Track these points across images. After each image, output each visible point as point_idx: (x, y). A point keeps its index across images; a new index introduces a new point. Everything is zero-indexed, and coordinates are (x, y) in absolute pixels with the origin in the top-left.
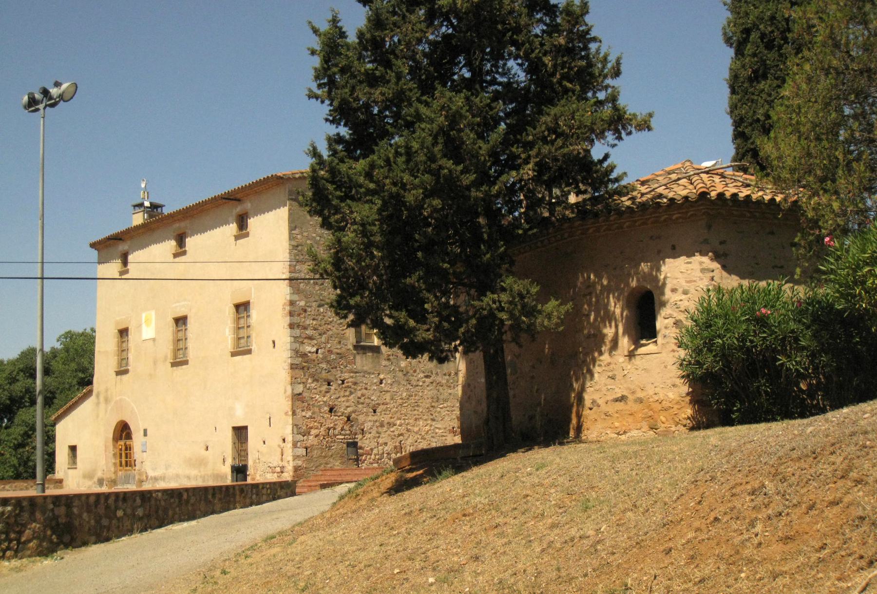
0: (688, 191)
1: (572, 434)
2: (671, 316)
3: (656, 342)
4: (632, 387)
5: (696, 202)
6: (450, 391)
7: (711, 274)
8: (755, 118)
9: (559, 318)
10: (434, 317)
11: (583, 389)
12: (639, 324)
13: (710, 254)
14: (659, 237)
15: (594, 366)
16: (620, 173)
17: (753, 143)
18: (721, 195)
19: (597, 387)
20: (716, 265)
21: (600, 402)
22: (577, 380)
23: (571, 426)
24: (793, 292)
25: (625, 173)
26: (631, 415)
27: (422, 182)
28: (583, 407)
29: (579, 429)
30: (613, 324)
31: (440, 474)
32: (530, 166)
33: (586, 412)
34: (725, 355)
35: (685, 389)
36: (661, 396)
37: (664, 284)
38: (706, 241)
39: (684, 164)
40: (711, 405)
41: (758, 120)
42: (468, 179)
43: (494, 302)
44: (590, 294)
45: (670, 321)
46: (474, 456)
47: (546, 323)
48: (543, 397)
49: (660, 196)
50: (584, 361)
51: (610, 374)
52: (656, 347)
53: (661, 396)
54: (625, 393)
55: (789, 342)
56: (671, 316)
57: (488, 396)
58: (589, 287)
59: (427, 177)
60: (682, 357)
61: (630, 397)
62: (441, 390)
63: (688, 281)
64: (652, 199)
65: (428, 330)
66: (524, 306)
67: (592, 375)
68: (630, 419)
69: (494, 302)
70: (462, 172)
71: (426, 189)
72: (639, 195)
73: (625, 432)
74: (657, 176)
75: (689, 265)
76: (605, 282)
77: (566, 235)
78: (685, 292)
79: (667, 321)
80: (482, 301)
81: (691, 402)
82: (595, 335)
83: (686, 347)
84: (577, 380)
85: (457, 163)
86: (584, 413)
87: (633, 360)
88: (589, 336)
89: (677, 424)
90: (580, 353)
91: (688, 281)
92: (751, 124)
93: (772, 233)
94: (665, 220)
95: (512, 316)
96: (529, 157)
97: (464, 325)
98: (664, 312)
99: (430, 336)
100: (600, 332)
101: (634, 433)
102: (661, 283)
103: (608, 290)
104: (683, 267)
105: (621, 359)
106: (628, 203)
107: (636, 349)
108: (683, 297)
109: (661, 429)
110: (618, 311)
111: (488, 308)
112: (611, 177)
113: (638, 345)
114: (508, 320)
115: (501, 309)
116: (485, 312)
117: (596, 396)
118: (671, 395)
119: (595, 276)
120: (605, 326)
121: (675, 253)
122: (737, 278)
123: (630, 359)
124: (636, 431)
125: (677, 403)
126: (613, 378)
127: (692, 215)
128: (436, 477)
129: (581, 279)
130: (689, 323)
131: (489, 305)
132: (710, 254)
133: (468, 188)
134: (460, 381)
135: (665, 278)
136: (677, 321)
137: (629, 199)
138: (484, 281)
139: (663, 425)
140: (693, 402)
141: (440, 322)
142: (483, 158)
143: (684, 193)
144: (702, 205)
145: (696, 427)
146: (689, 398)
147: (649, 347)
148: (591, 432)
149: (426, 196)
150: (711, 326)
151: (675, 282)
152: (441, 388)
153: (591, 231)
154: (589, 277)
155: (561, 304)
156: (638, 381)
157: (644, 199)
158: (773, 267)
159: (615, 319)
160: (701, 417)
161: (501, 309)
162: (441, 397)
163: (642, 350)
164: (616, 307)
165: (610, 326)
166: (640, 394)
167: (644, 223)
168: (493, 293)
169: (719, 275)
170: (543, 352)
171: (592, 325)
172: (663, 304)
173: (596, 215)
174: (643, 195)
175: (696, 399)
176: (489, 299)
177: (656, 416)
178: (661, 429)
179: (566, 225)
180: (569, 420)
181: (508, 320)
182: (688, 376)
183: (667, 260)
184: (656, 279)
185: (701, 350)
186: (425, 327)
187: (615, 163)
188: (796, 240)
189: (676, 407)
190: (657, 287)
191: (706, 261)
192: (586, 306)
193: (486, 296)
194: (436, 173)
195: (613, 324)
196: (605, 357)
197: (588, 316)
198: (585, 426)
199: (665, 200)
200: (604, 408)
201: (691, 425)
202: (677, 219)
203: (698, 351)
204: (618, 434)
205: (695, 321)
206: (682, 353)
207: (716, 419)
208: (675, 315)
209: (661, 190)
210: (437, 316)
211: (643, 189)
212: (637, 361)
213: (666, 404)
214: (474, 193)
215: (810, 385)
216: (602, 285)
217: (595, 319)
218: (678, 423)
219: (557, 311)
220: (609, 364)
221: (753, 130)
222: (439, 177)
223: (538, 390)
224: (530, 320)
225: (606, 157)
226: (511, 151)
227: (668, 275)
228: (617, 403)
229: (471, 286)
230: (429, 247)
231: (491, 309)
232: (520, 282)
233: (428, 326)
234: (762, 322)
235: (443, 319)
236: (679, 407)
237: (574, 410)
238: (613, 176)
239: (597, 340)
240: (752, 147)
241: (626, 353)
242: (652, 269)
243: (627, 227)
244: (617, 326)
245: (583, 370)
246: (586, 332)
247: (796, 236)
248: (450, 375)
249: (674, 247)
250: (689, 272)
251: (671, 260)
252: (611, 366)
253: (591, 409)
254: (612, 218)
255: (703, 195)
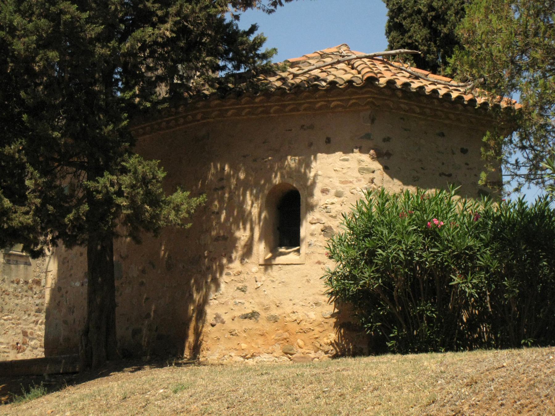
0: (351, 76)
1: (187, 353)
2: (319, 222)
3: (298, 251)
4: (266, 302)
5: (361, 88)
6: (17, 301)
7: (372, 175)
8: (416, 9)
9: (188, 212)
10: (36, 197)
11: (205, 301)
12: (278, 229)
13: (372, 152)
14: (312, 127)
15: (221, 274)
16: (270, 49)
17: (410, 37)
18: (391, 83)
19: (223, 300)
20: (377, 166)
21: (225, 317)
22: (198, 290)
23: (187, 345)
24: (462, 207)
25: (275, 50)
26: (262, 335)
27: (37, 29)
28: (203, 323)
29: (196, 349)
30: (248, 226)
31: (28, 391)
32: (168, 26)
33: (207, 329)
34: (385, 270)
35: (330, 309)
36: (300, 316)
37: (314, 183)
38: (368, 136)
39: (339, 48)
40: (362, 329)
41: (419, 12)
42: (94, 30)
43: (112, 185)
44: (223, 188)
45: (318, 227)
46: (66, 373)
47: (172, 217)
48: (153, 307)
49: (317, 78)
50: (209, 268)
51: (240, 285)
52: (298, 257)
53: (300, 316)
54: (256, 309)
55: (465, 260)
56: (319, 222)
57: (90, 301)
58: (222, 179)
59: (43, 22)
60: (332, 270)
61: (263, 314)
62: (7, 299)
63: (344, 181)
64: (308, 81)
65: (27, 213)
66: (148, 193)
67: (218, 286)
68: (260, 341)
69: (112, 185)
70: (88, 21)
71: (40, 37)
72: (291, 77)
73: (253, 356)
74: (309, 58)
75: (346, 163)
76: (242, 176)
77: (199, 117)
78: (338, 195)
79: (313, 227)
80: (98, 183)
81: (336, 325)
82: (225, 238)
83: (340, 259)
84: (198, 290)
85: (82, 9)
86: (204, 330)
87: (269, 271)
88: (217, 238)
89: (317, 350)
90: (205, 257)
91: (344, 181)
92: (410, 15)
93: (442, 135)
94: (320, 108)
95: (133, 204)
96: (167, 14)
97: (74, 211)
98: (310, 217)
99: (28, 220)
100: (232, 234)
101: (265, 358)
102: (309, 183)
103: (245, 185)
104: (339, 164)
105: (255, 269)
106: (279, 84)
107: (273, 258)
108: (336, 200)
109: (297, 355)
110: (255, 211)
111: (104, 191)
112: (259, 52)
113: (276, 254)
114: (127, 207)
115: (120, 193)
116: (100, 196)
117: (221, 311)
118: (312, 315)
119: (231, 167)
120: (238, 228)
121: (329, 147)
122: (400, 183)
123: (266, 270)
124: (267, 356)
125: (319, 325)
126: (243, 290)
127: (354, 104)
128: (23, 394)
129: (213, 171)
130: (344, 230)
131: (106, 187)
132: (372, 152)
133: (92, 41)
134: (49, 285)
135: (316, 176)
136: (326, 228)
137: (278, 80)
138: (102, 157)
139: (300, 350)
140: (339, 325)
141: (43, 204)
142: (113, 7)
143: (348, 77)
144: (366, 93)
145: (341, 352)
146: (334, 320)
147: (291, 257)
148: (212, 353)
149: (39, 47)
150: (370, 235)
151: (327, 181)
152: (7, 297)
153: (230, 113)
154: (223, 169)
155: (190, 197)
156: (273, 297)
157: (297, 81)
158: (440, 175)
159: (251, 220)
160: (348, 344)
161: (120, 193)
162: (6, 307)
163: (280, 260)
164: (253, 207)
165: (245, 229)
166: (275, 312)
167: (296, 109)
168: (112, 174)
169: (380, 178)
170: (159, 254)
171: (222, 226)
172: (311, 208)
173: (239, 94)
174: (295, 76)
175: (343, 323)
176: (105, 180)
177: (292, 339)
178: (297, 355)
179: (201, 104)
180: (185, 337)
181: (127, 207)
182: (337, 293)
183: (319, 155)
184: (304, 177)
185: (358, 263)
186: (26, 209)
187: (265, 36)
188: (485, 139)
189: (317, 329)
190: (306, 187)
191: (366, 159)
192: (216, 203)
193: (102, 176)
194: (55, 18)
195: (248, 226)
196: (236, 265)
197: (218, 214)
198: (204, 345)
199: (324, 84)
200: (230, 325)
201: (334, 352)
202: (336, 107)
203: (355, 264)
204: (244, 357)
205: (351, 228)
206: (332, 265)
207: (365, 347)
208: (324, 220)
209: (316, 72)
210: (39, 197)
211: (294, 70)
212: (274, 272)
213: (305, 325)
214: (100, 50)
215: (471, 315)
216: (238, 179)
217: (227, 219)
218: (318, 349)
219: (188, 203)
220: (239, 273)
221: (412, 22)
222: (59, 23)
223: (147, 299)
224: (154, 211)
225: (253, 29)
226: (145, 6)
227: (320, 173)
228: (246, 321)
229: (81, 166)
230: (36, 111)
231: (108, 192)
232: (146, 163)
233: (28, 209)
234: (432, 235)
235: (46, 200)
236: (321, 330)
237: (192, 325)
238: (261, 50)
239: (227, 244)
240: (409, 41)
241: (261, 262)
242: (300, 163)
243: (275, 112)
244: (252, 230)
245: (207, 278)
246: (214, 233)
247: (485, 135)
248: (18, 283)
249: (328, 141)
250: (344, 171)
251: (324, 155)
252: (242, 276)
253: (213, 325)
254: (257, 100)
255: (371, 81)
